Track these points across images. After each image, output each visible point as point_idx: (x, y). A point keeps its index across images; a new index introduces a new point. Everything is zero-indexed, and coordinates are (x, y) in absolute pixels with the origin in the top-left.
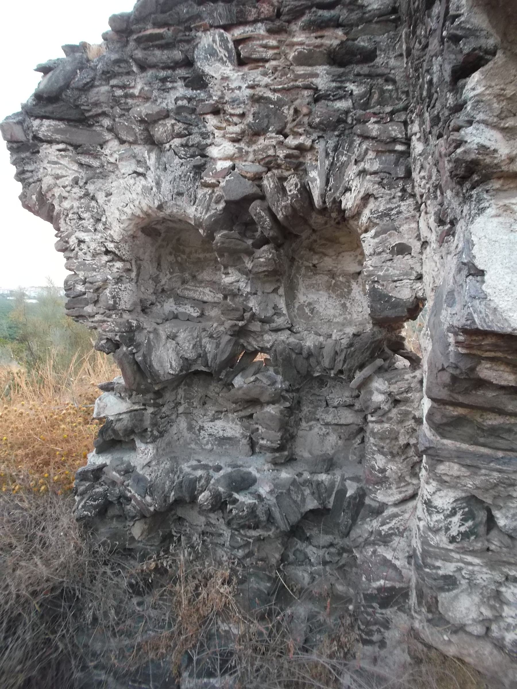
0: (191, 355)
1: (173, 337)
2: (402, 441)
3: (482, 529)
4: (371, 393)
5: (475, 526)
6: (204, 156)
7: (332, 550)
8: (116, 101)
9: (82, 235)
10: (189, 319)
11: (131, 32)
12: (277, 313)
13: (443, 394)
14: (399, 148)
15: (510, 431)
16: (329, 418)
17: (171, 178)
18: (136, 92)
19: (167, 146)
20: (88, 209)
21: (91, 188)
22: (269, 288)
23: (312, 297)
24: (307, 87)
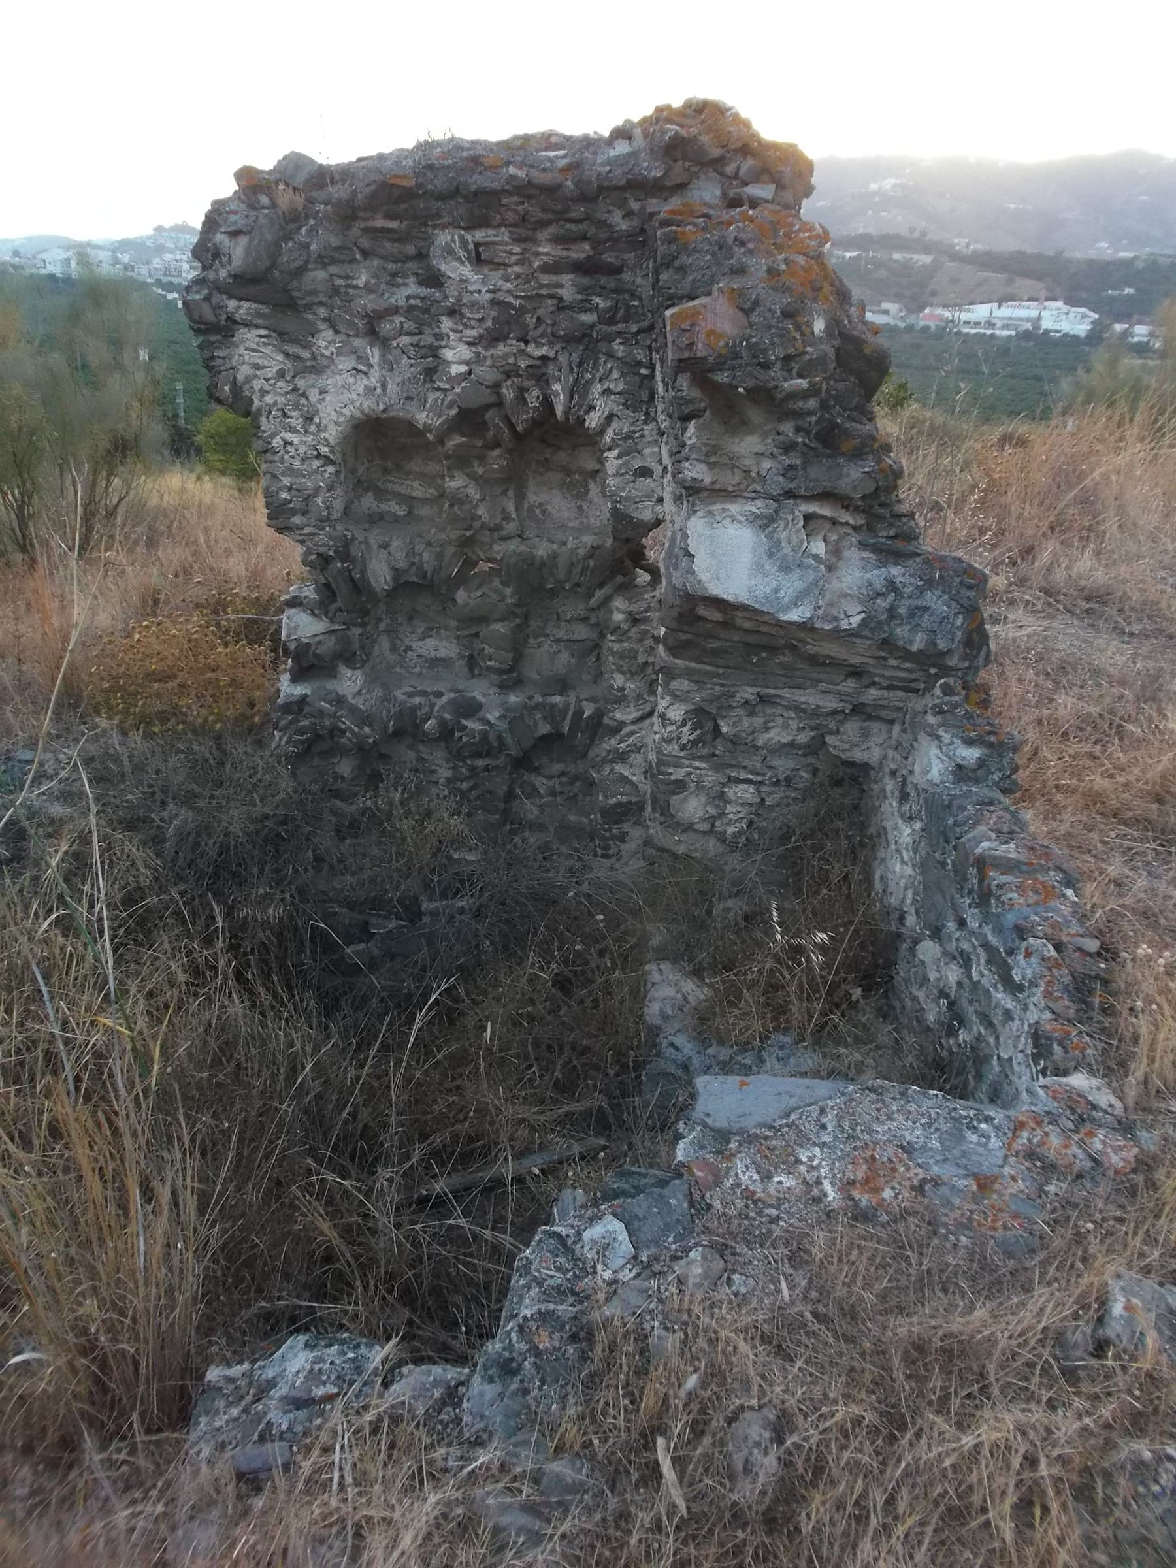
0: (402, 565)
1: (385, 546)
2: (641, 659)
3: (709, 737)
4: (611, 612)
5: (703, 734)
6: (435, 356)
7: (564, 779)
8: (336, 291)
9: (289, 436)
10: (396, 519)
11: (354, 218)
12: (507, 518)
13: (674, 625)
14: (643, 371)
15: (726, 652)
16: (561, 634)
17: (399, 380)
18: (361, 282)
19: (394, 344)
20: (296, 407)
21: (301, 383)
22: (498, 490)
23: (543, 497)
24: (552, 296)
